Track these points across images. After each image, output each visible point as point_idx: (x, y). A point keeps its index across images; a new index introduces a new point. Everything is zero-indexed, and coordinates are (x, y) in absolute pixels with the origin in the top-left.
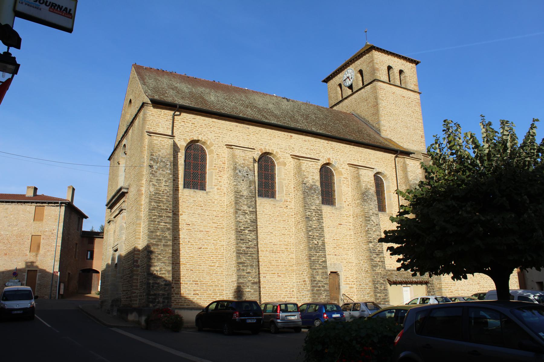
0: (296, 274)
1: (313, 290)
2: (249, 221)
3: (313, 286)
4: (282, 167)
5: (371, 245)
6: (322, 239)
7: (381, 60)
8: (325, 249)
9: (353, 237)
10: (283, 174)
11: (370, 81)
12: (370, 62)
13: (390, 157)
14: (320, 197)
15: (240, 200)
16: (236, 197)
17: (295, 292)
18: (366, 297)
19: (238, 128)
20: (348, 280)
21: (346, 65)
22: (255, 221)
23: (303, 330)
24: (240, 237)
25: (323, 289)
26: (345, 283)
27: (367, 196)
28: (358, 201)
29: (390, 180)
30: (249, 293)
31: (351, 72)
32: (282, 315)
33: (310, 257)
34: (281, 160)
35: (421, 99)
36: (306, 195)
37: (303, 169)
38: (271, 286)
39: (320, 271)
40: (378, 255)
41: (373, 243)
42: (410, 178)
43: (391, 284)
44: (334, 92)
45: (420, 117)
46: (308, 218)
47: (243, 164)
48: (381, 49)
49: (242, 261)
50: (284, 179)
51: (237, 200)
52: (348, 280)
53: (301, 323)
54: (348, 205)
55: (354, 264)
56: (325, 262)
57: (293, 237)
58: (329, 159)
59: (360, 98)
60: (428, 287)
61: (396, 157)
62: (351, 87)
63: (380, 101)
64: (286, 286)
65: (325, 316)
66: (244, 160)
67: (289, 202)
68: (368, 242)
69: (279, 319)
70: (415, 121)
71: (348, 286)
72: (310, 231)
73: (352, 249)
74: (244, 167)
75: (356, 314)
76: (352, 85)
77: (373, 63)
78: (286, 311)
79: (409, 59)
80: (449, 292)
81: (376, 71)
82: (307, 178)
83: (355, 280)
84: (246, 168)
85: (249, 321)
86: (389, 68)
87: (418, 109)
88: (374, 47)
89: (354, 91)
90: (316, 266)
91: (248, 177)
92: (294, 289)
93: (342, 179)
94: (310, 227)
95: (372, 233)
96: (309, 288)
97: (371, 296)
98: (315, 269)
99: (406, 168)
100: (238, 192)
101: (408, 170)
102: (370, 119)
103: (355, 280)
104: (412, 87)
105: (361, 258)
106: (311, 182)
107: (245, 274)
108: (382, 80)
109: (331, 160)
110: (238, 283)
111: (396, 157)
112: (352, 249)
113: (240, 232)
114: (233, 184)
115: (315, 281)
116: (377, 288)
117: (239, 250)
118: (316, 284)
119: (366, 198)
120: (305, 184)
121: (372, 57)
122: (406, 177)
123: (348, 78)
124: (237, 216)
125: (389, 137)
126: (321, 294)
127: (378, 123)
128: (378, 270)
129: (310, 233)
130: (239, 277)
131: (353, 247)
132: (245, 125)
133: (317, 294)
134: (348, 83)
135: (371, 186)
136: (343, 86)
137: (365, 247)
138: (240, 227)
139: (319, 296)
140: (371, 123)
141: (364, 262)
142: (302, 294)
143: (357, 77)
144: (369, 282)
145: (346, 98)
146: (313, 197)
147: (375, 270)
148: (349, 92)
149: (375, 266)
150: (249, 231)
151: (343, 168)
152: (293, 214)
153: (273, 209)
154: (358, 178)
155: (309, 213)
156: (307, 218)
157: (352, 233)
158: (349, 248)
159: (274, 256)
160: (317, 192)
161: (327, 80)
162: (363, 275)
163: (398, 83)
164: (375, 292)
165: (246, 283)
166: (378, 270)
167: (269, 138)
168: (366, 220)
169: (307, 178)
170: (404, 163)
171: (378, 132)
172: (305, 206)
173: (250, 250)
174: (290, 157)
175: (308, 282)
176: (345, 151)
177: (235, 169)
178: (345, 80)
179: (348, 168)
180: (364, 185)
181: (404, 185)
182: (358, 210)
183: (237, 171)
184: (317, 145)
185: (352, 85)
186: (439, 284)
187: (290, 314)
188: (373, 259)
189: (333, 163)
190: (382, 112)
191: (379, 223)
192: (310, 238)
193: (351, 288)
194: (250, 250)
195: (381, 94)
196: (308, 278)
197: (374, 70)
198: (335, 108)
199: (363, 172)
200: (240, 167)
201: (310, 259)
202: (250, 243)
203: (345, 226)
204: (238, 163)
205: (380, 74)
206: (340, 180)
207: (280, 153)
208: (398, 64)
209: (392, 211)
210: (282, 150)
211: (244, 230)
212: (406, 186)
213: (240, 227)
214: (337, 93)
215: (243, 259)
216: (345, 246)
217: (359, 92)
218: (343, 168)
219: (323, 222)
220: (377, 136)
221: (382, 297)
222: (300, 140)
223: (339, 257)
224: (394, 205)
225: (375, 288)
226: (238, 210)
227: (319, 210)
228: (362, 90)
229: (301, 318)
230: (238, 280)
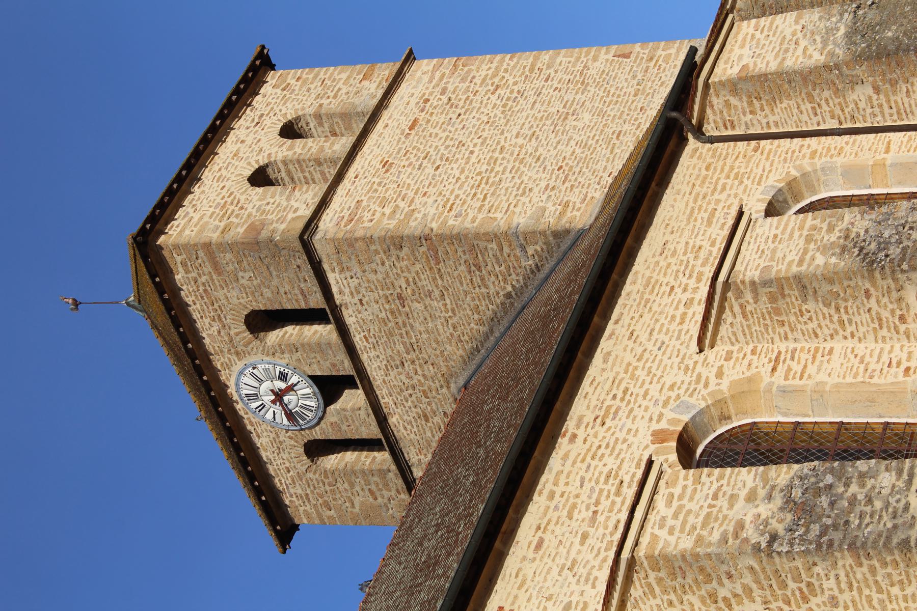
7: (219, 205)
11: (307, 272)
12: (216, 266)
13: (693, 158)
14: (862, 465)
21: (222, 417)
27: (883, 245)
29: (819, 163)
31: (262, 379)
36: (837, 536)
37: (687, 543)
42: (818, 58)
44: (343, 486)
45: (526, 59)
58: (659, 437)
59: (390, 334)
61: (699, 132)
62: (330, 388)
63: (414, 226)
70: (538, 84)
76: (319, 381)
77: (223, 247)
79: (237, 91)
81: (264, 234)
82: (740, 525)
86: (261, 178)
87: (483, 67)
88: (143, 231)
89: (346, 368)
93: (779, 379)
99: (763, 78)
101: (773, 66)
102: (499, 288)
104: (373, 89)
106: (764, 510)
108: (307, 213)
109: (663, 425)
111: (699, 132)
120: (774, 537)
121: (191, 249)
122: (807, 80)
123: (279, 396)
125: (598, 194)
127: (520, 239)
134: (305, 397)
135: (831, 229)
136: (318, 434)
140: (516, 279)
143: (281, 349)
145: (382, 419)
146: (853, 501)
148: (352, 399)
151: (720, 374)
154: (786, 292)
160: (829, 479)
161: (284, 529)
169: (740, 525)
170: (733, 86)
171: (562, 240)
176: (628, 357)
178: (290, 415)
179: (721, 348)
180: (820, 260)
181: (852, 96)
184: (573, 489)
189: (686, 418)
190: (470, 219)
195: (379, 219)
197: (257, 248)
198: (418, 473)
199: (750, 264)
205: (281, 220)
206: (783, 391)
208: (252, 139)
212: (855, 82)
214: (349, 473)
217: (358, 340)
218: (720, 374)
220: (585, 243)
222: (528, 570)
228: (350, 320)
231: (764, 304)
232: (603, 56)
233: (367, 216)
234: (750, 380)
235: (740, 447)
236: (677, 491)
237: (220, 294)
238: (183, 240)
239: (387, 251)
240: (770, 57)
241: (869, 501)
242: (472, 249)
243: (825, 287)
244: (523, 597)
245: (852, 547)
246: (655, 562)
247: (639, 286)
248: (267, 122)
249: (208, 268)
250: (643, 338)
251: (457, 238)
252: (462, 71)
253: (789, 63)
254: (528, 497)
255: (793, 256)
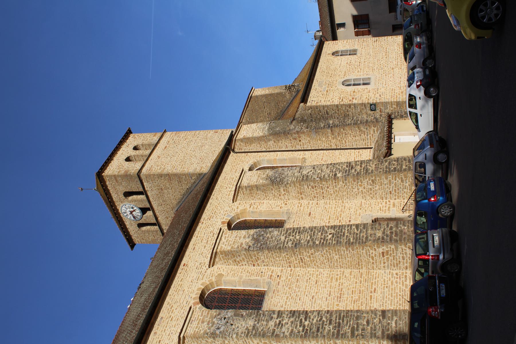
0: (373, 268)
1: (396, 241)
2: (292, 319)
3: (391, 240)
4: (223, 278)
5: (339, 175)
6: (326, 228)
8: (340, 226)
9: (328, 201)
10: (233, 278)
11: (139, 182)
12: (117, 181)
13: (232, 157)
15: (260, 330)
16: (255, 335)
17: (398, 271)
18: (407, 184)
19: (159, 332)
20: (384, 208)
22: (293, 313)
23: (454, 228)
24: (313, 333)
25: (394, 229)
26: (387, 212)
27: (276, 178)
28: (282, 190)
29: (261, 159)
30: (398, 322)
31: (127, 209)
32: (431, 253)
33: (349, 244)
34: (214, 279)
35: (172, 130)
36: (264, 246)
37: (229, 248)
38: (389, 302)
39: (369, 231)
40: (352, 168)
41: (337, 173)
42: (261, 134)
43: (391, 154)
45: (193, 132)
46: (297, 245)
47: (208, 324)
48: (103, 166)
49: (350, 330)
50: (241, 277)
51: (260, 335)
52: (384, 208)
53: (444, 230)
54: (286, 204)
55: (363, 201)
56: (357, 226)
57: (322, 270)
60: (396, 118)
61: (233, 151)
62: (144, 211)
63: (165, 172)
64: (390, 282)
65: (433, 199)
66: (203, 322)
67: (272, 272)
68: (335, 179)
69: (438, 256)
71: (391, 209)
72: (314, 243)
73: (343, 202)
74: (213, 323)
75: (430, 168)
76: (141, 209)
77: (118, 176)
78: (426, 249)
79: (123, 138)
80: (402, 96)
81: (129, 173)
82: (242, 244)
83: (385, 201)
84: (215, 320)
85: (443, 293)
86: (128, 159)
87: (183, 134)
88: (99, 172)
89: (148, 206)
90: (363, 237)
91: (229, 318)
92: (394, 272)
93: (251, 209)
94: (308, 242)
95: (323, 174)
96: (393, 247)
97: (406, 177)
98: (367, 238)
99: (249, 138)
100: (248, 333)
101: (251, 136)
102: (185, 187)
103: (385, 201)
104: (156, 139)
105: (356, 190)
106: (247, 240)
107: (369, 328)
109: (224, 220)
110: (383, 338)
111: (233, 151)
112: (343, 202)
113: (306, 332)
114: (235, 340)
115: (383, 238)
116: (395, 168)
117: (333, 335)
118: (387, 236)
119: (278, 179)
120: (250, 247)
121: (107, 176)
124: (282, 335)
126: (401, 231)
127: (191, 175)
128: (372, 167)
129: (317, 242)
130: (373, 335)
131: (340, 201)
132: (157, 323)
133: (401, 236)
134: (138, 213)
135: (264, 174)
136: (141, 222)
137: (341, 183)
138: (299, 332)
139: (405, 233)
141: (361, 186)
142: (401, 260)
143: (132, 201)
144: (387, 178)
145: (156, 218)
147: (372, 170)
148: (149, 213)
149: (367, 170)
150: (306, 320)
151: (238, 208)
152: (289, 269)
153: (280, 293)
154: (253, 189)
155: (290, 244)
156: (295, 246)
157: (322, 201)
158: (342, 206)
159: (346, 296)
160: (263, 233)
161: (132, 244)
162: (378, 187)
163: (148, 152)
164: (400, 171)
165: (383, 326)
166: (372, 167)
167: (181, 293)
168: (307, 179)
169: (242, 244)
170: (242, 140)
171: (201, 176)
172: (280, 248)
173: (334, 319)
174: (212, 269)
175: (383, 248)
176: (216, 204)
177: (214, 335)
178: (134, 217)
179: (238, 202)
180: (261, 181)
181: (269, 143)
182: (293, 191)
183: (218, 332)
184: (202, 235)
185: (141, 209)
186: (392, 104)
187: (430, 242)
188: (358, 173)
189: (229, 218)
190: (179, 170)
191: (311, 166)
192: (324, 243)
193: (394, 205)
194: (334, 319)
195: (157, 170)
196: (378, 247)
197: (127, 176)
199: (245, 182)
200: (212, 328)
201: (352, 243)
202: (324, 319)
203: (313, 209)
204: (206, 331)
206: (252, 212)
207: (204, 281)
209: (299, 159)
210: (201, 277)
211: (304, 326)
212: (270, 140)
213: (299, 332)
214: (148, 231)
215: (347, 329)
216: (339, 210)
217: (151, 199)
218: (238, 208)
219: (304, 227)
220: (206, 177)
221: (407, 164)
222: (191, 255)
223: (353, 217)
224: (292, 156)
225: (395, 171)
226: (273, 333)
227: (287, 231)
229: (436, 229)
230: (378, 338)
231: (248, 192)
232: (211, 132)
233: (154, 169)
234: (244, 209)
235: (256, 293)
236: (227, 236)
237: (117, 187)
238: (108, 174)
239: (158, 178)
240: (250, 134)
241: (272, 238)
242: (179, 177)
243: (262, 188)
244: (190, 261)
245: (268, 249)
246: (222, 253)
247: (219, 187)
248: (130, 146)
249: (115, 181)
250: (220, 199)
251: (176, 175)
252: (177, 135)
253: (254, 135)
254: (191, 237)
255: (255, 180)
